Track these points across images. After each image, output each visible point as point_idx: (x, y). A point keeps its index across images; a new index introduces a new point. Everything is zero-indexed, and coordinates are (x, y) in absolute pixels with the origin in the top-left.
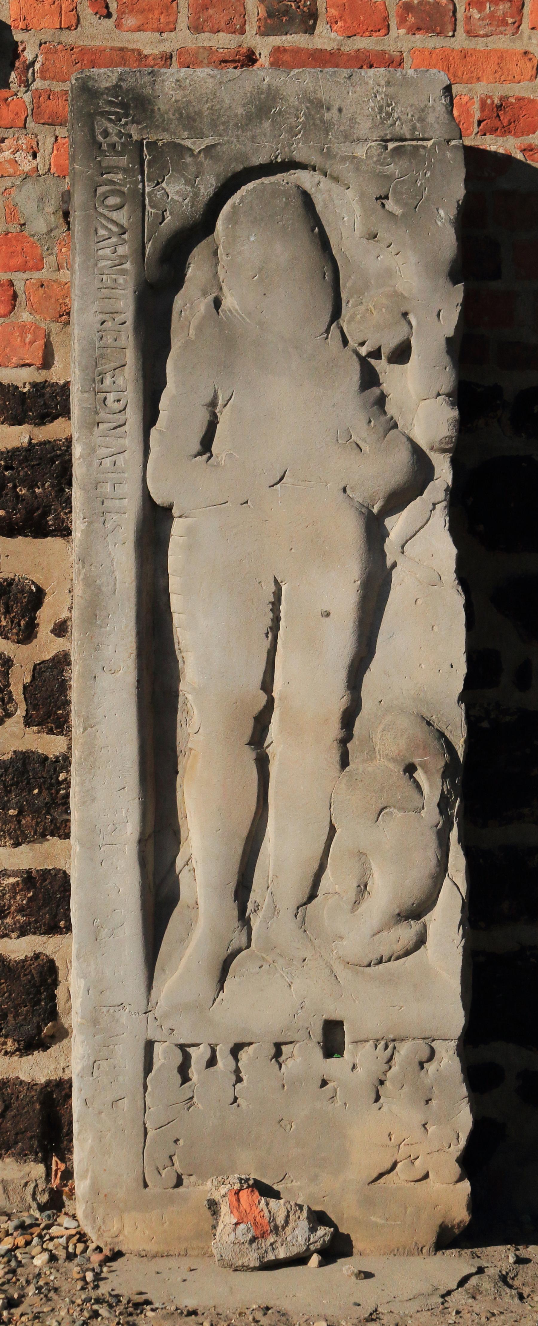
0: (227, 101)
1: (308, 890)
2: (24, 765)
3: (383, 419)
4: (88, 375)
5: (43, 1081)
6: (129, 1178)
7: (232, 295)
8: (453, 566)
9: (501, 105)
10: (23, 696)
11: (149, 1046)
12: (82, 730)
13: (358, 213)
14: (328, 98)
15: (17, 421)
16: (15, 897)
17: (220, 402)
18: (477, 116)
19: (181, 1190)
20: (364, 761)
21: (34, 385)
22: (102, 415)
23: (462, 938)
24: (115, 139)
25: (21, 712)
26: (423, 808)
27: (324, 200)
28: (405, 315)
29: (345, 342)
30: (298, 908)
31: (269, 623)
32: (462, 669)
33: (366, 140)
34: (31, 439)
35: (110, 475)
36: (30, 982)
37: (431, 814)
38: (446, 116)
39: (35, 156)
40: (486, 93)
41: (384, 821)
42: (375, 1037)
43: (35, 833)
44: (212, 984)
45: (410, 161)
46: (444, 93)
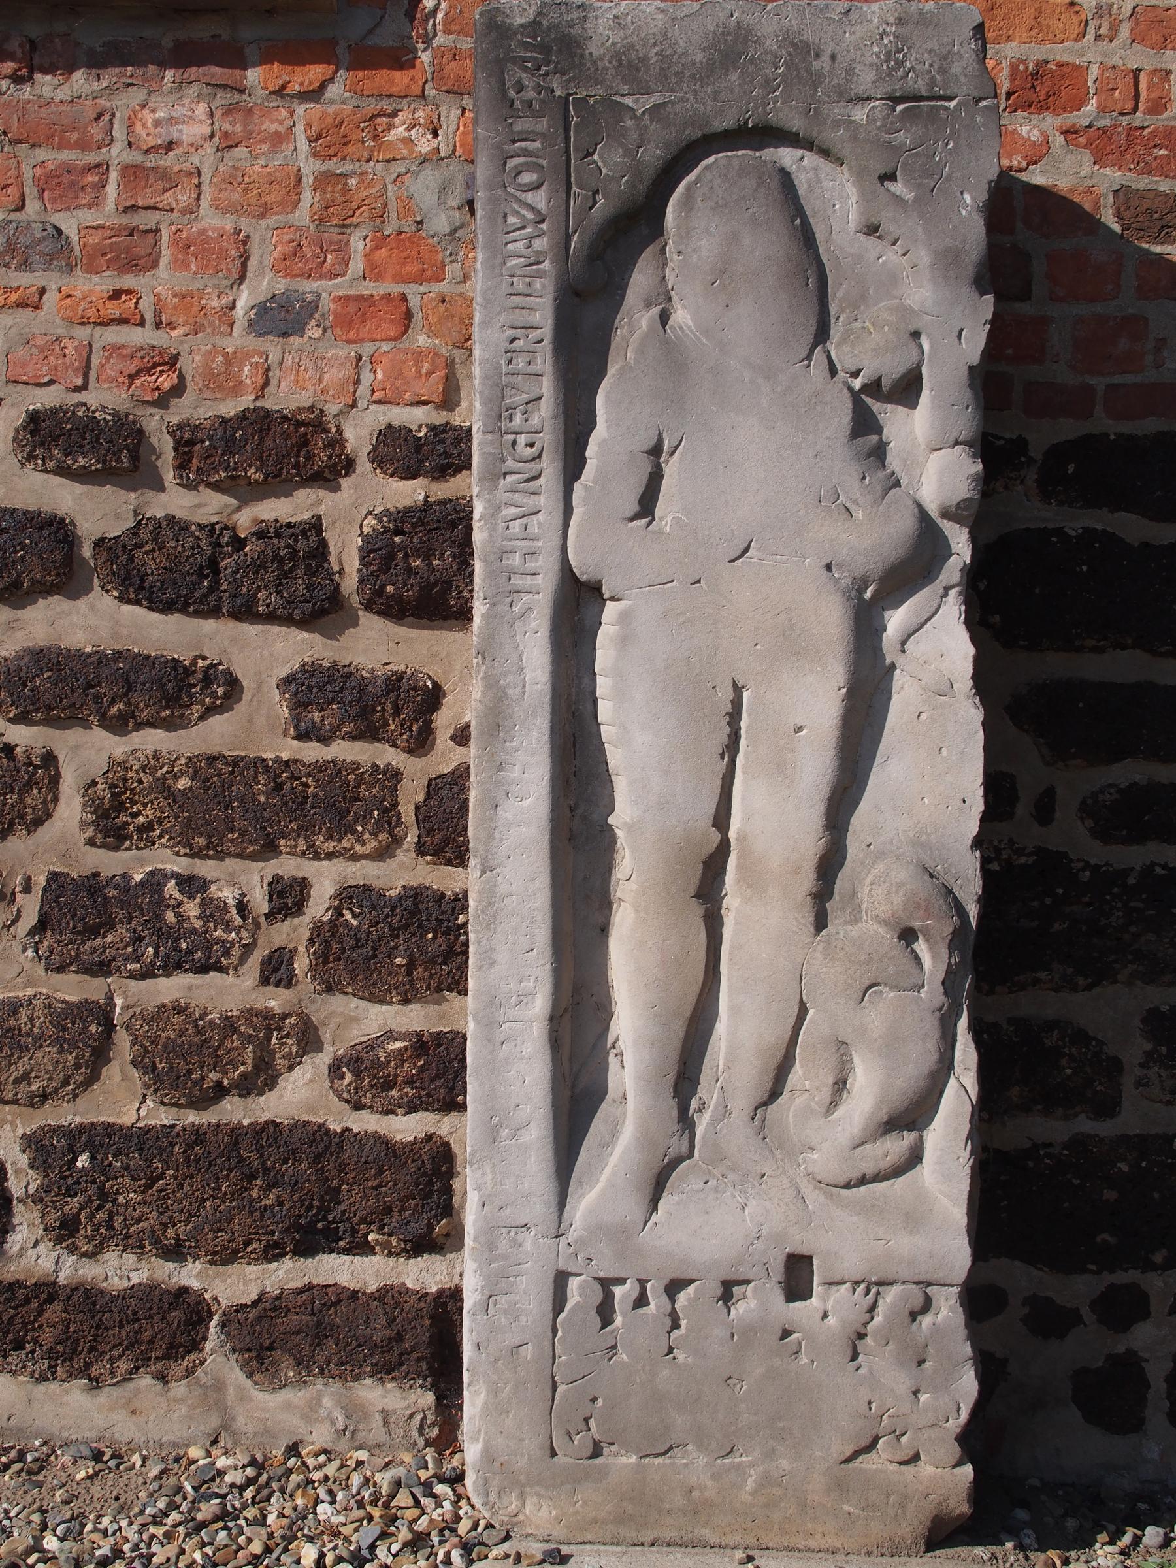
0: (682, 44)
1: (769, 1086)
2: (415, 904)
3: (880, 474)
4: (492, 409)
5: (434, 1289)
6: (533, 1444)
7: (684, 307)
8: (970, 670)
9: (1038, 72)
10: (414, 818)
11: (561, 1279)
12: (479, 873)
13: (853, 199)
14: (817, 41)
15: (410, 474)
16: (402, 1066)
17: (666, 447)
18: (1005, 86)
19: (599, 1461)
20: (846, 923)
21: (432, 428)
22: (510, 464)
23: (971, 1155)
24: (531, 94)
25: (411, 838)
26: (923, 986)
27: (809, 182)
28: (916, 335)
29: (833, 371)
30: (756, 1109)
31: (725, 740)
32: (977, 805)
33: (868, 99)
34: (427, 496)
35: (519, 543)
36: (420, 1169)
37: (932, 994)
38: (977, 67)
39: (435, 134)
40: (1017, 56)
41: (871, 1002)
42: (853, 1279)
43: (428, 988)
44: (645, 1204)
45: (926, 127)
46: (974, 35)
